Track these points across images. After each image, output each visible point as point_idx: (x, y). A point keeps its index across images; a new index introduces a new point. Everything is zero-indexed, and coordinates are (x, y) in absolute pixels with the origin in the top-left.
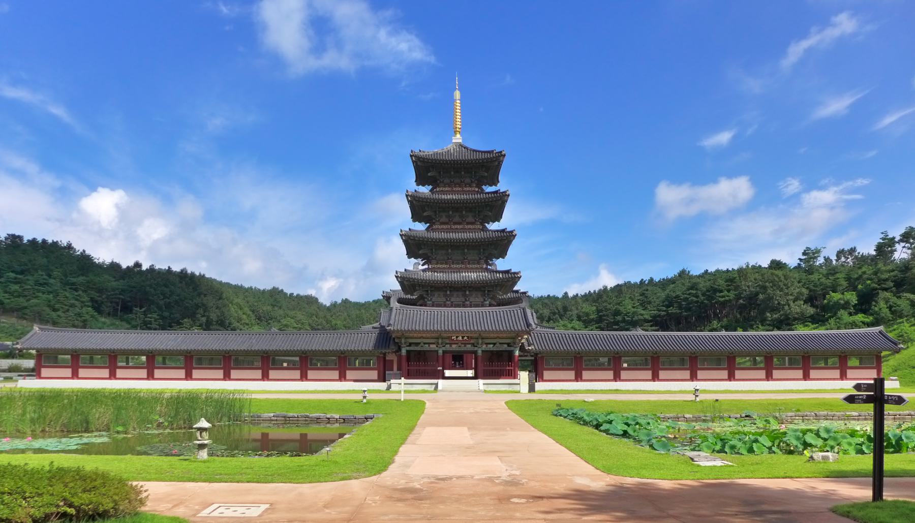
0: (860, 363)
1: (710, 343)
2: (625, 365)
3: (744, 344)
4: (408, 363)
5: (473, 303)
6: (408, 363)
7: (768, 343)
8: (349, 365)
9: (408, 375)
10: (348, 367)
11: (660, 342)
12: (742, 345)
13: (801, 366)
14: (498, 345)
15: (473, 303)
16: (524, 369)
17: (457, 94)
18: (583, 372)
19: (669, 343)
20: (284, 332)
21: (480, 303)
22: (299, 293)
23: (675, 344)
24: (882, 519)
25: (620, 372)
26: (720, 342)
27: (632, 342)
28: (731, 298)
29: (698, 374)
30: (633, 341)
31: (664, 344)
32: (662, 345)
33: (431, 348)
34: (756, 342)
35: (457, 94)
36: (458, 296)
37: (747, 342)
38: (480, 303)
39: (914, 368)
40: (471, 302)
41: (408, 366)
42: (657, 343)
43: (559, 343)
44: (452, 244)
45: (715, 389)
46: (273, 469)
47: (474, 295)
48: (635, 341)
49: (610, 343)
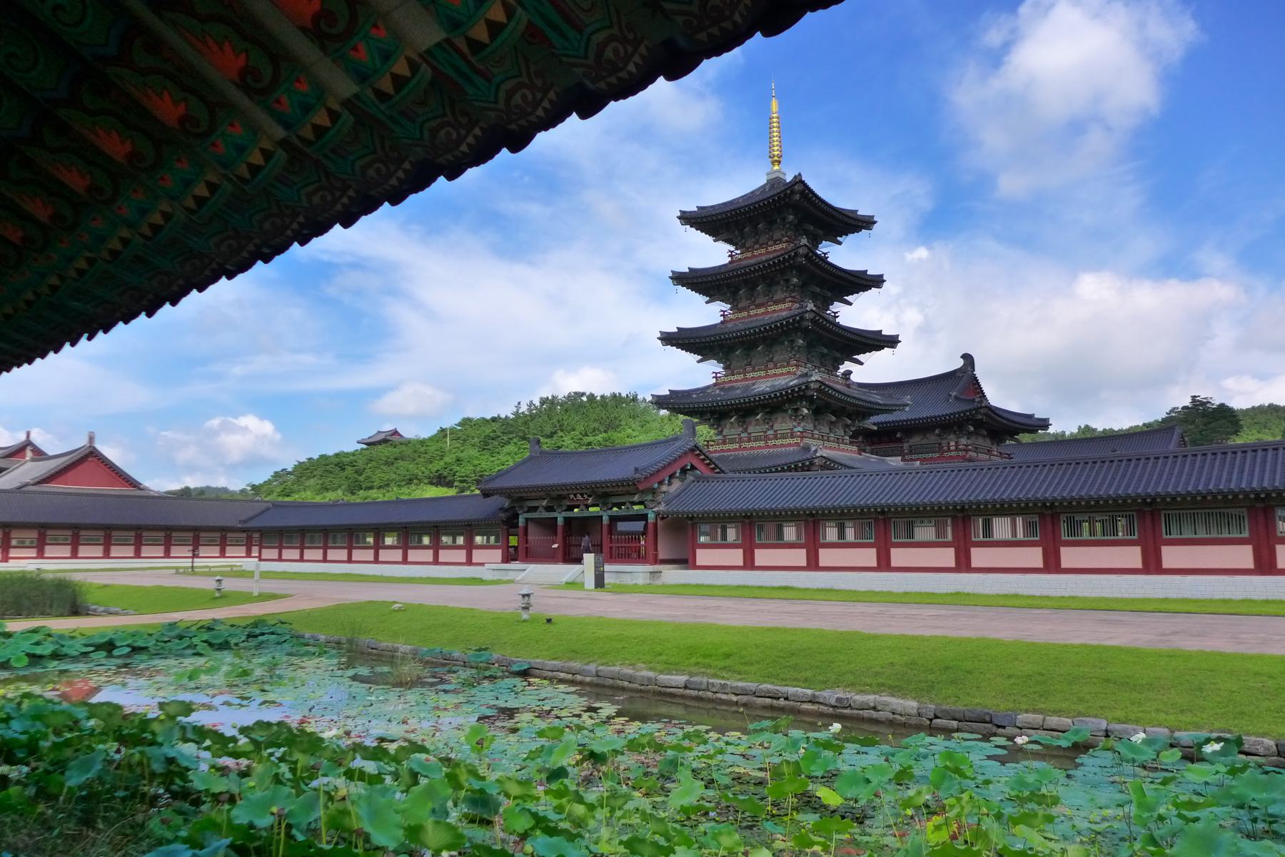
0: (938, 536)
2: (702, 539)
4: (611, 538)
5: (779, 432)
6: (611, 538)
8: (358, 543)
9: (611, 558)
10: (757, 542)
13: (1038, 539)
15: (779, 432)
16: (588, 551)
17: (774, 105)
18: (820, 550)
20: (977, 463)
21: (789, 431)
22: (1203, 394)
24: (895, 707)
35: (774, 105)
36: (783, 422)
38: (789, 431)
40: (776, 431)
41: (611, 542)
44: (785, 329)
45: (447, 575)
47: (779, 420)
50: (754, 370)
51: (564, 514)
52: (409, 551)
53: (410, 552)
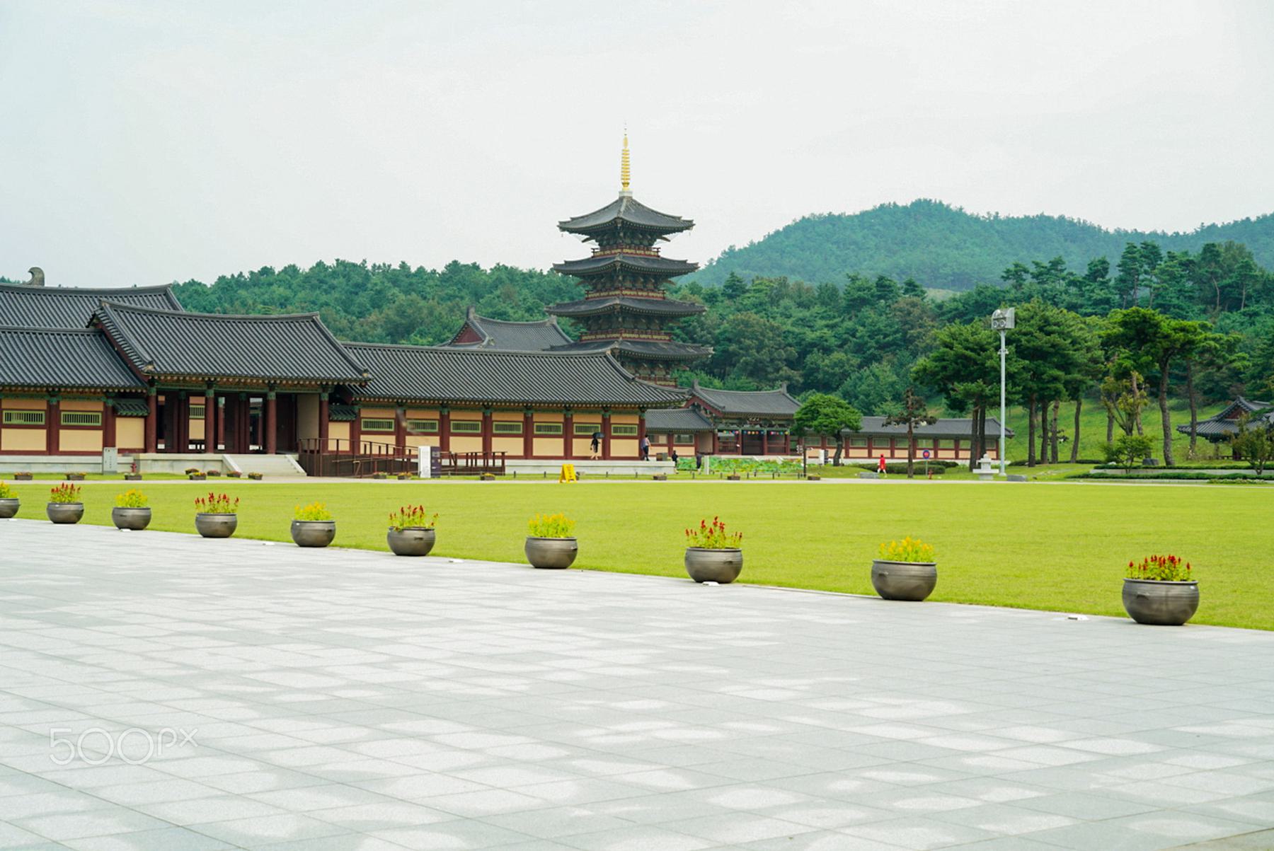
1: (36, 372)
3: (80, 370)
7: (60, 317)
11: (23, 358)
12: (33, 355)
14: (1031, 477)
19: (163, 357)
23: (33, 364)
25: (405, 439)
26: (36, 372)
27: (93, 370)
28: (1142, 379)
29: (1027, 455)
30: (55, 348)
31: (14, 354)
32: (49, 376)
33: (394, 411)
34: (34, 374)
37: (51, 312)
39: (2, 713)
42: (9, 374)
43: (29, 358)
46: (833, 420)
48: (64, 320)
49: (23, 363)
50: (625, 332)
51: (768, 429)
52: (613, 442)
53: (939, 452)
